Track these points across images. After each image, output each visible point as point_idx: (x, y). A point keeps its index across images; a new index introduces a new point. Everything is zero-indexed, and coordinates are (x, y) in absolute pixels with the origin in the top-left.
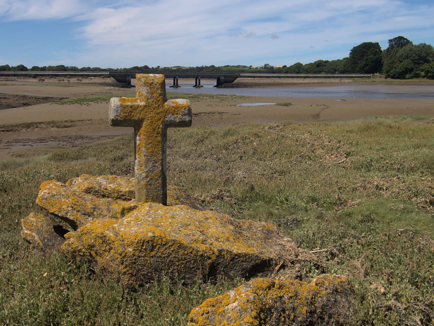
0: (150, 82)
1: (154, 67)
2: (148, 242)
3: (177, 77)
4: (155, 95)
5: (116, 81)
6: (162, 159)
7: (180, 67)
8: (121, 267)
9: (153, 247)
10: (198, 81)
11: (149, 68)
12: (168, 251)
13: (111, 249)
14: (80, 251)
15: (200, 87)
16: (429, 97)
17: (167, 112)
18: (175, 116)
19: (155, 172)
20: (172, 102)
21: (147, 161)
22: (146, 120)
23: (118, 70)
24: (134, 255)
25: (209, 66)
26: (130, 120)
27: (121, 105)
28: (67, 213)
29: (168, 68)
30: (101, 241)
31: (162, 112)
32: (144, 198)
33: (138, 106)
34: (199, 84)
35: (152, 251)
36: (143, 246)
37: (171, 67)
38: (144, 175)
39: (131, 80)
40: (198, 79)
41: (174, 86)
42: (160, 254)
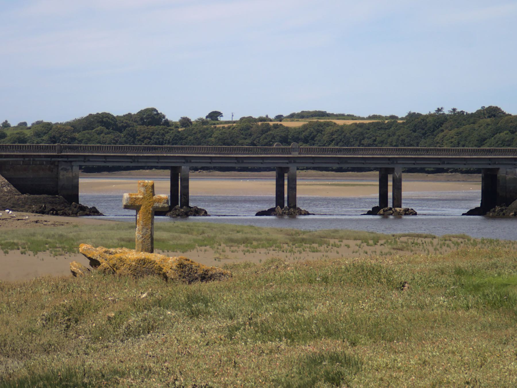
0: (146, 185)
1: (193, 118)
2: (142, 260)
3: (292, 167)
4: (148, 192)
5: (11, 188)
6: (151, 228)
7: (322, 114)
8: (129, 271)
9: (144, 264)
10: (390, 183)
11: (167, 123)
12: (151, 266)
13: (124, 264)
14: (108, 268)
15: (399, 215)
16: (444, 198)
17: (154, 201)
18: (159, 204)
19: (147, 235)
20: (158, 196)
21: (143, 228)
22: (143, 206)
23: (8, 132)
24: (135, 266)
25: (471, 109)
26: (134, 205)
27: (130, 198)
28: (97, 258)
29: (261, 119)
30: (119, 261)
31: (152, 201)
32: (140, 249)
33: (139, 198)
34: (398, 200)
35: (144, 265)
36: (139, 262)
37: (279, 118)
38: (141, 236)
39: (81, 181)
40: (390, 178)
41: (279, 210)
42: (147, 267)
